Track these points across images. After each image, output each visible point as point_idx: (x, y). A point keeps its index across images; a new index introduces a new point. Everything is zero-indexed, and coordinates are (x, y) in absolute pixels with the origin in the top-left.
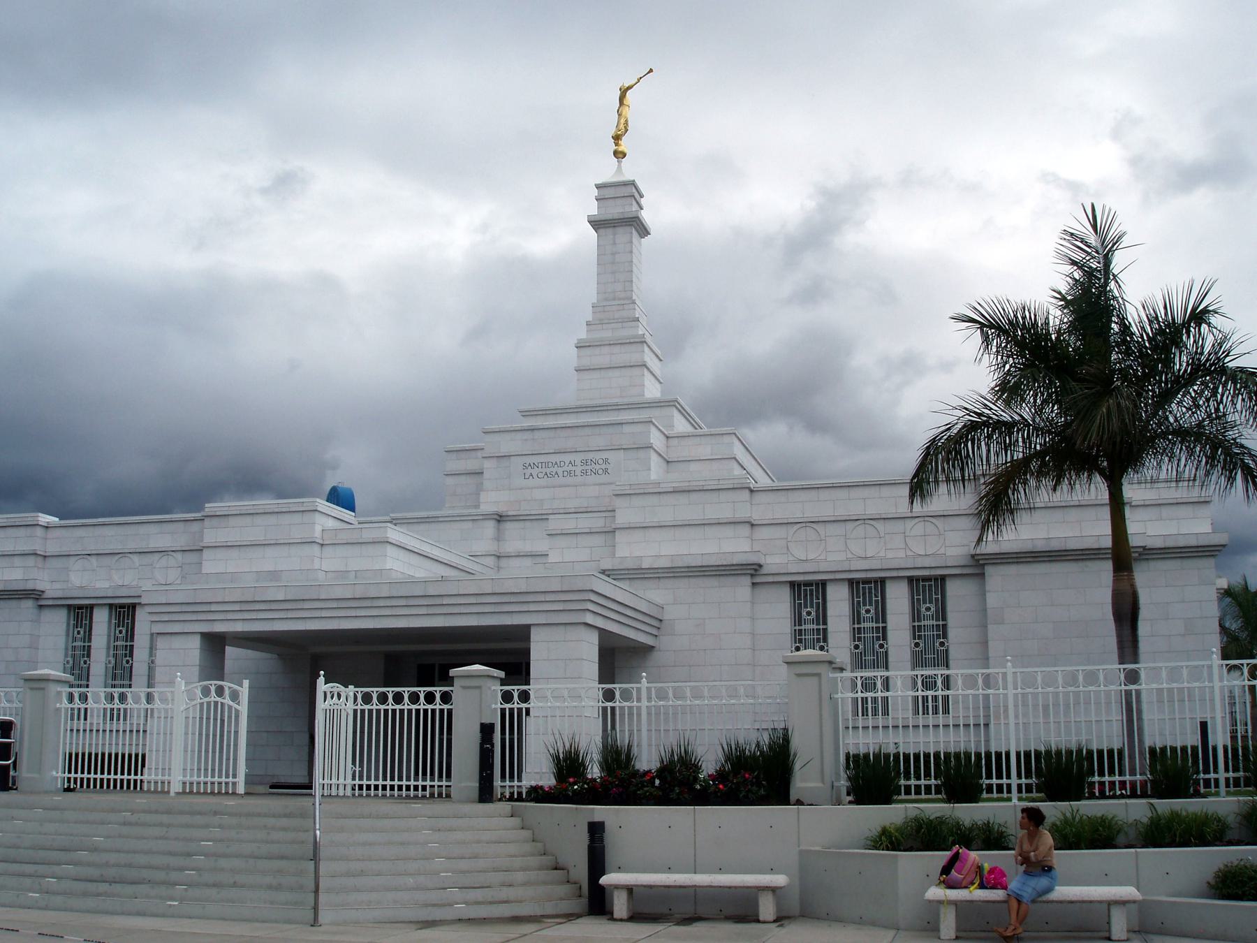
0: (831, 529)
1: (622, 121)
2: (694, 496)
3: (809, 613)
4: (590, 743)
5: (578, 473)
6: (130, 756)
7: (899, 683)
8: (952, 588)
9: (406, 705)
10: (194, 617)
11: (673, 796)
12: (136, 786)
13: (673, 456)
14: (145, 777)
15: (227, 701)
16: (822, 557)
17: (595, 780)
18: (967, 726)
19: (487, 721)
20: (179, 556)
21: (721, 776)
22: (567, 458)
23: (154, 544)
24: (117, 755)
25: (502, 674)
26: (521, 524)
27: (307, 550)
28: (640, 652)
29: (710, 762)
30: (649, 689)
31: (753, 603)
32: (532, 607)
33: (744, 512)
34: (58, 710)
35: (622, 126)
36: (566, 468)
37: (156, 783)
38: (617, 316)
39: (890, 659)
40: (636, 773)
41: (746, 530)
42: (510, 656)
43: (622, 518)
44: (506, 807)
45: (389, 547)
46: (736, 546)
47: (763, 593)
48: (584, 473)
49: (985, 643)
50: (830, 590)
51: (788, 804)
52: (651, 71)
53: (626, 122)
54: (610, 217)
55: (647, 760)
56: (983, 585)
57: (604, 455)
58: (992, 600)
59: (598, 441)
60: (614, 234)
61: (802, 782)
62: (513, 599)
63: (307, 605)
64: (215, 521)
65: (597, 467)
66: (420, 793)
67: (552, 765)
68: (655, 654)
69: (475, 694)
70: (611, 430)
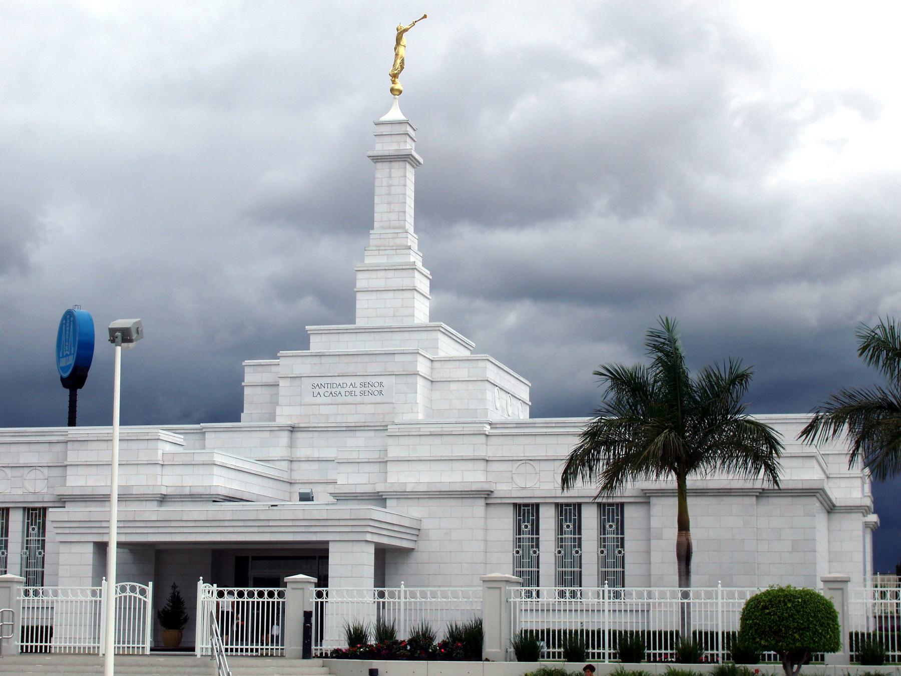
0: (544, 465)
1: (399, 61)
2: (445, 439)
3: (526, 527)
4: (369, 624)
5: (358, 393)
6: (42, 627)
7: (545, 593)
8: (628, 512)
9: (246, 599)
10: (89, 531)
11: (417, 655)
12: (46, 651)
13: (436, 377)
14: (53, 644)
15: (138, 596)
16: (537, 486)
17: (371, 646)
18: (631, 611)
19: (308, 610)
20: (45, 470)
21: (444, 644)
22: (349, 381)
23: (22, 461)
24: (42, 627)
25: (315, 580)
26: (310, 435)
27: (151, 469)
28: (404, 553)
29: (441, 635)
30: (405, 591)
31: (486, 518)
32: (330, 529)
33: (482, 452)
34: (18, 601)
35: (398, 65)
36: (347, 389)
37: (60, 648)
38: (391, 244)
39: (583, 562)
40: (396, 642)
41: (481, 465)
42: (312, 559)
43: (393, 453)
44: (320, 661)
45: (215, 468)
46: (474, 477)
47: (493, 511)
48: (363, 393)
49: (648, 552)
50: (542, 510)
51: (481, 660)
52: (425, 16)
53: (403, 62)
54: (386, 153)
55: (403, 635)
56: (649, 510)
57: (379, 379)
58: (655, 523)
59: (374, 367)
60: (390, 169)
61: (490, 646)
62: (317, 523)
63: (173, 524)
64: (76, 445)
65: (374, 389)
66: (254, 653)
67: (346, 637)
68: (414, 554)
69: (298, 591)
70: (385, 358)
